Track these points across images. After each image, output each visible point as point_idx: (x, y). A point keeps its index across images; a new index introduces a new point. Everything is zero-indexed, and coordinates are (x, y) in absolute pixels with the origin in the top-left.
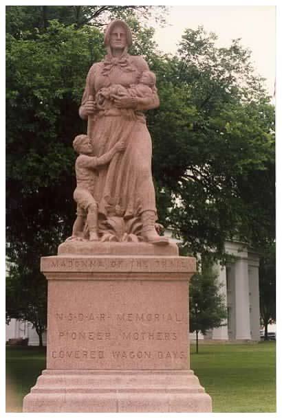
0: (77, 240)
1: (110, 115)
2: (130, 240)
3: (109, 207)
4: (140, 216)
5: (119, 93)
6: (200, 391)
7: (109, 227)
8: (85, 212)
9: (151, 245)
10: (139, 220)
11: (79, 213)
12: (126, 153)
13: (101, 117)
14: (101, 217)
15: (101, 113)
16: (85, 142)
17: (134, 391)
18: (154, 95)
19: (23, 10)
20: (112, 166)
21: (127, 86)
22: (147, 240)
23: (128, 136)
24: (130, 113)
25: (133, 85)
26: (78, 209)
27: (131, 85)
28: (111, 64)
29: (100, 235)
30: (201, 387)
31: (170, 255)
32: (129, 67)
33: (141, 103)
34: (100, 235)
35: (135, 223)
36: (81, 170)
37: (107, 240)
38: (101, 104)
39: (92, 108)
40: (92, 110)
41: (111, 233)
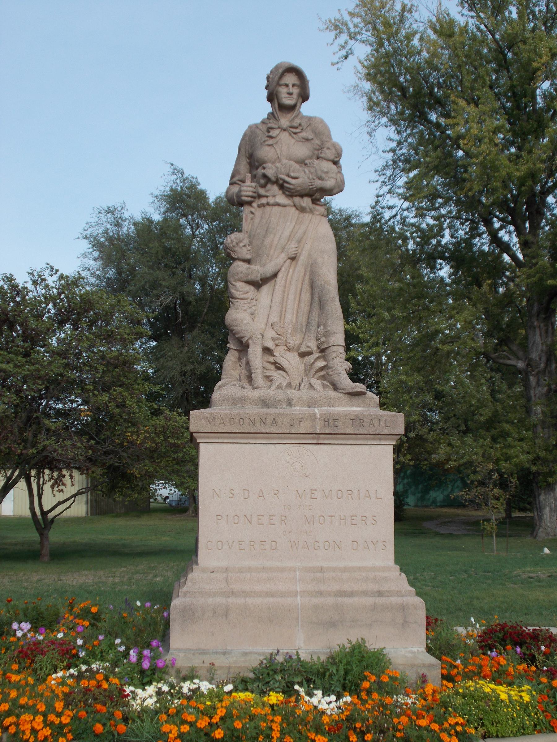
3: (278, 339)
4: (323, 351)
15: (264, 201)
16: (241, 244)
19: (196, 406)
23: (305, 233)
24: (306, 202)
25: (310, 161)
31: (353, 411)
32: (304, 134)
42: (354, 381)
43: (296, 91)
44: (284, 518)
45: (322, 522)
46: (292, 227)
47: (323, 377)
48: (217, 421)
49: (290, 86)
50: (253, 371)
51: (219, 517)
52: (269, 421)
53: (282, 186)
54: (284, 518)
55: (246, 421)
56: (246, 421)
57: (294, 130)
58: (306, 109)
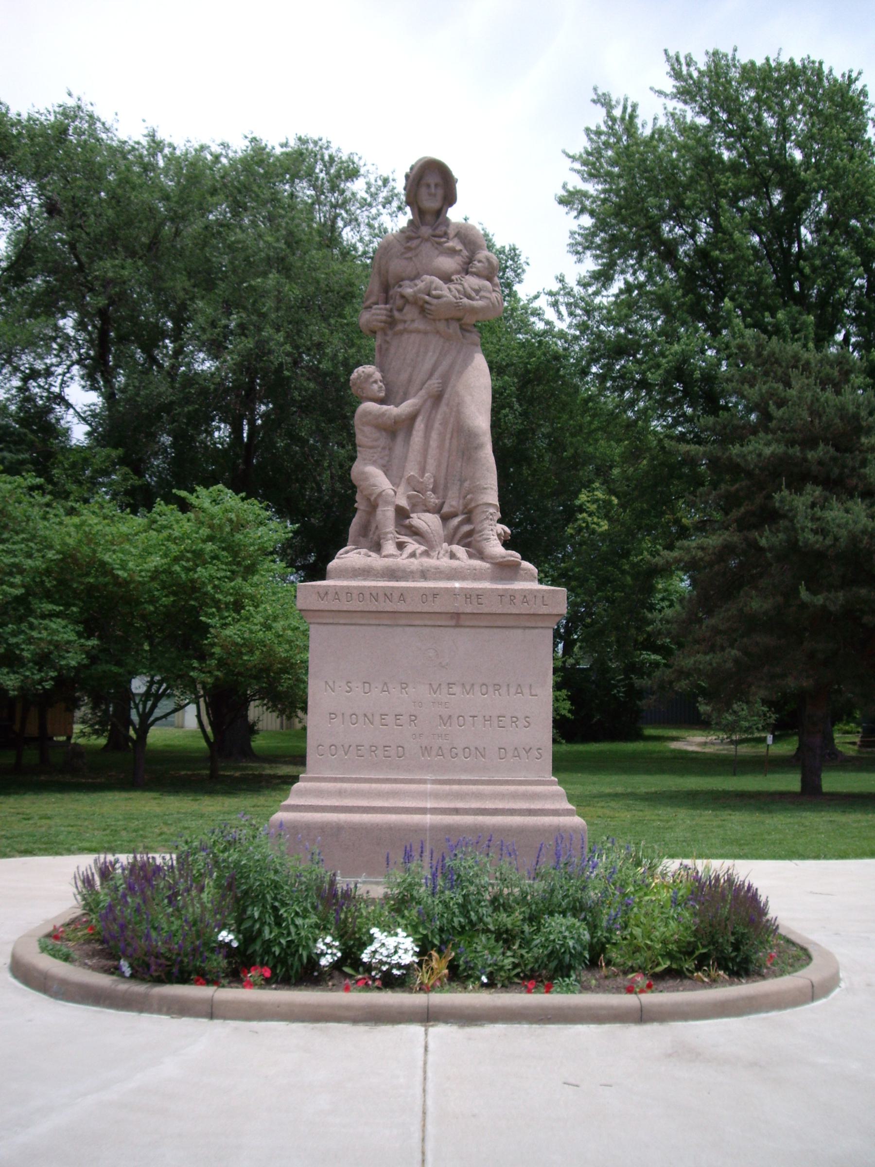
0: (359, 553)
1: (418, 331)
2: (453, 556)
4: (469, 515)
5: (434, 292)
6: (551, 783)
7: (415, 533)
8: (373, 507)
9: (488, 565)
10: (468, 520)
11: (360, 504)
12: (446, 396)
13: (401, 333)
14: (402, 514)
17: (457, 811)
18: (494, 294)
20: (419, 425)
21: (447, 279)
22: (480, 554)
25: (458, 276)
26: (358, 497)
27: (454, 277)
28: (418, 237)
29: (401, 546)
30: (570, 807)
33: (473, 310)
34: (401, 546)
35: (462, 523)
36: (367, 429)
37: (413, 555)
38: (400, 310)
39: (384, 318)
40: (385, 322)
41: (420, 543)
42: (507, 549)
43: (440, 192)
44: (413, 718)
45: (461, 723)
46: (435, 358)
47: (467, 545)
48: (330, 597)
49: (433, 186)
50: (382, 536)
51: (333, 716)
52: (396, 596)
53: (423, 310)
54: (413, 718)
55: (367, 596)
56: (367, 596)
57: (437, 239)
58: (454, 214)
